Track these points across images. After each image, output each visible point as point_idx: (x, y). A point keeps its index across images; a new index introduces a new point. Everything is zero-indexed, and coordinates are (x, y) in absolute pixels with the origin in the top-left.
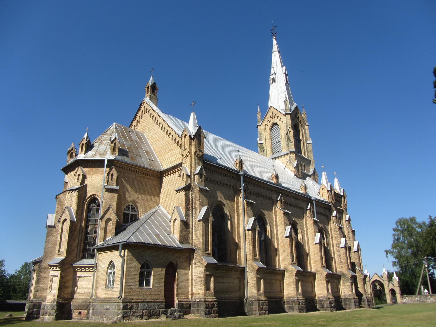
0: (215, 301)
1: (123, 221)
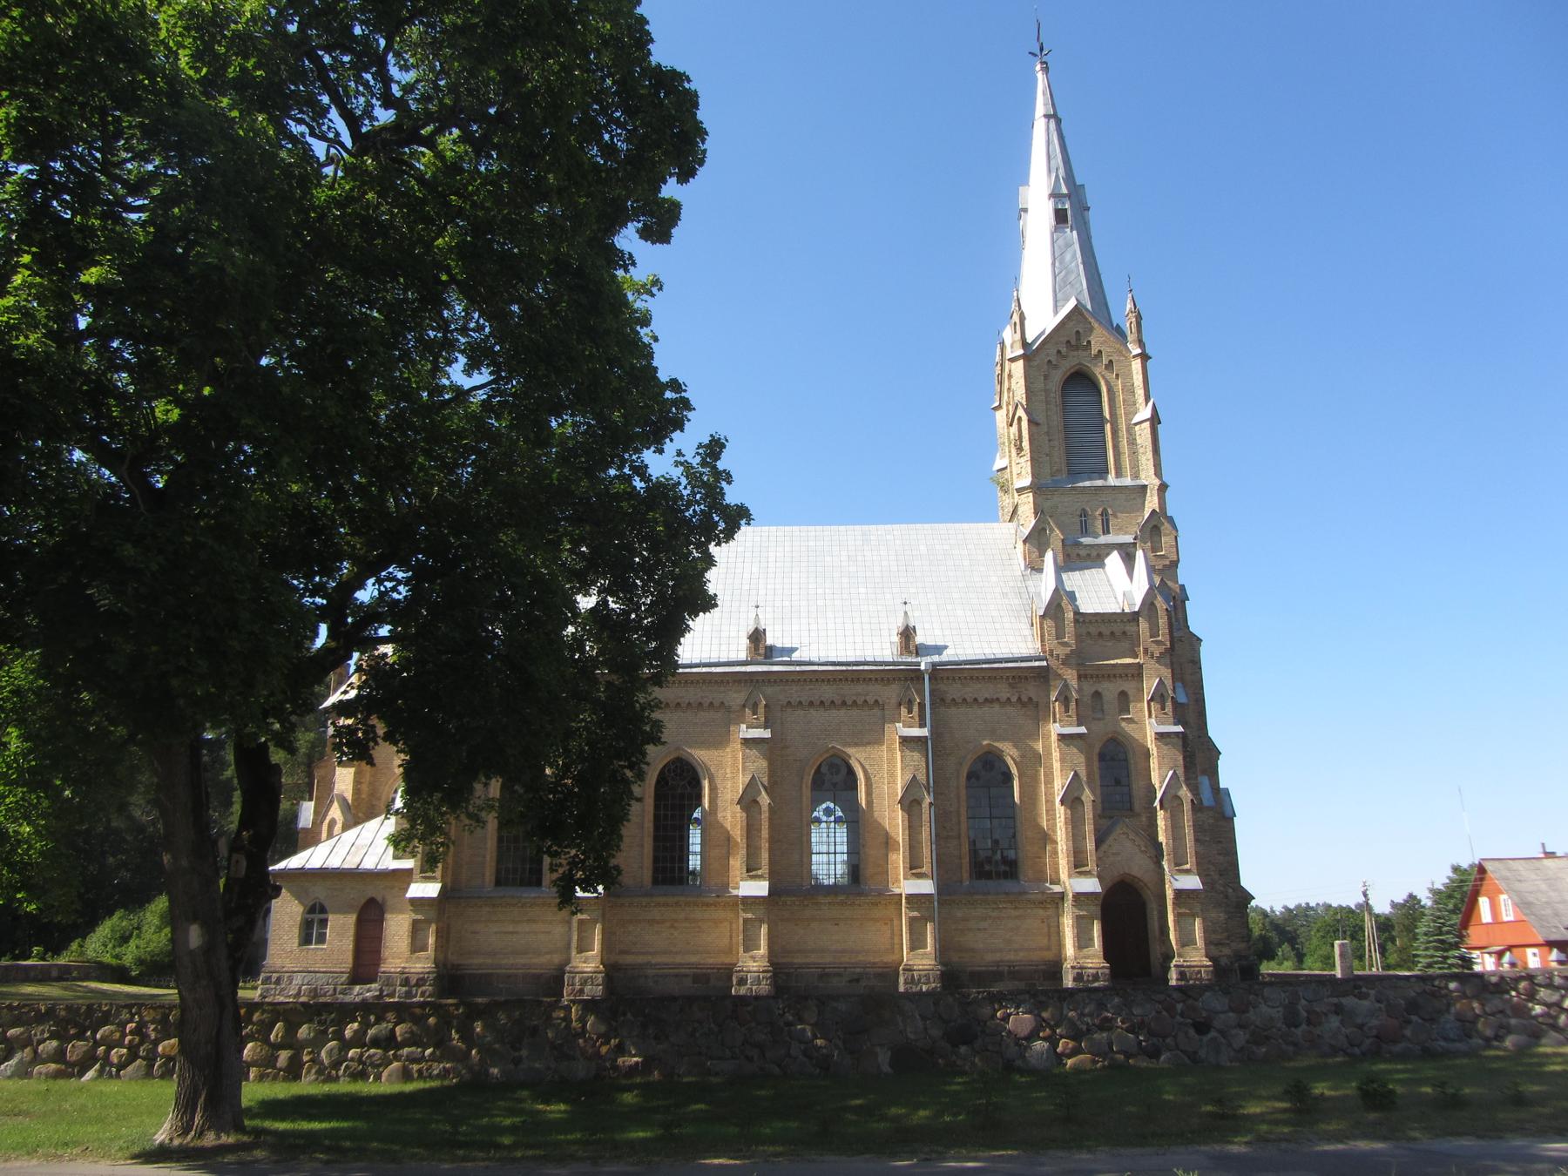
0: (428, 973)
1: (656, 870)
